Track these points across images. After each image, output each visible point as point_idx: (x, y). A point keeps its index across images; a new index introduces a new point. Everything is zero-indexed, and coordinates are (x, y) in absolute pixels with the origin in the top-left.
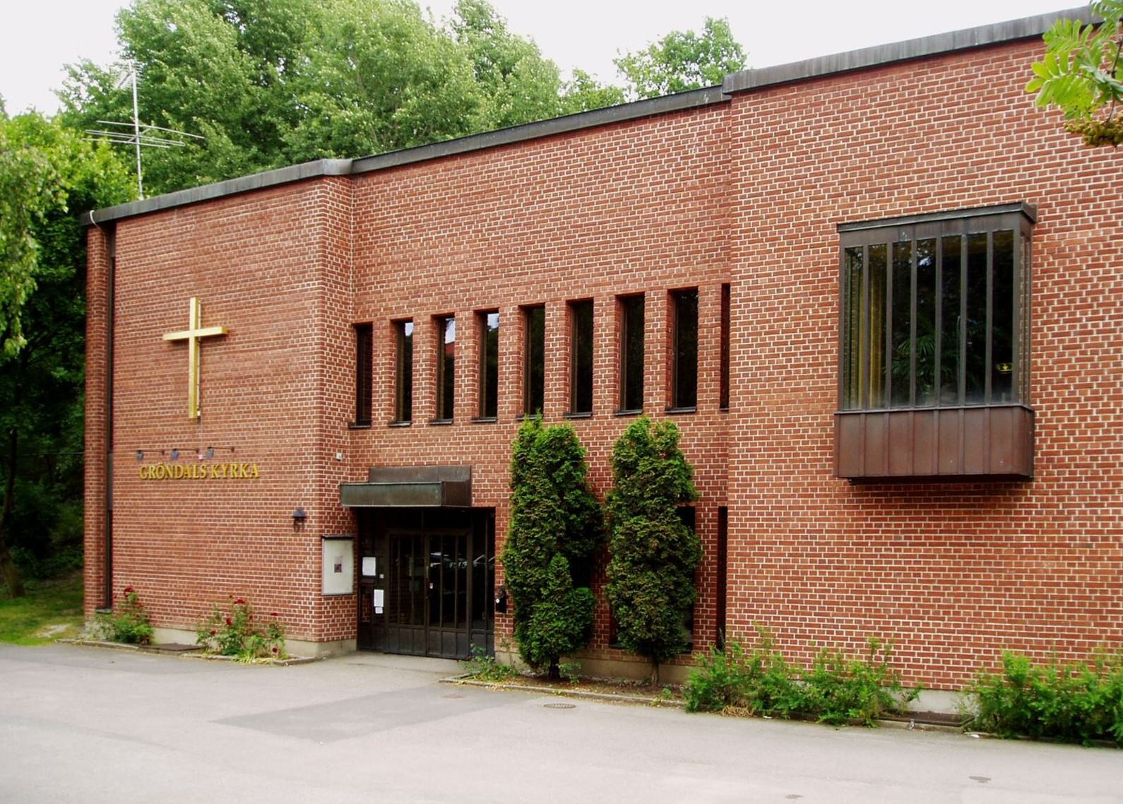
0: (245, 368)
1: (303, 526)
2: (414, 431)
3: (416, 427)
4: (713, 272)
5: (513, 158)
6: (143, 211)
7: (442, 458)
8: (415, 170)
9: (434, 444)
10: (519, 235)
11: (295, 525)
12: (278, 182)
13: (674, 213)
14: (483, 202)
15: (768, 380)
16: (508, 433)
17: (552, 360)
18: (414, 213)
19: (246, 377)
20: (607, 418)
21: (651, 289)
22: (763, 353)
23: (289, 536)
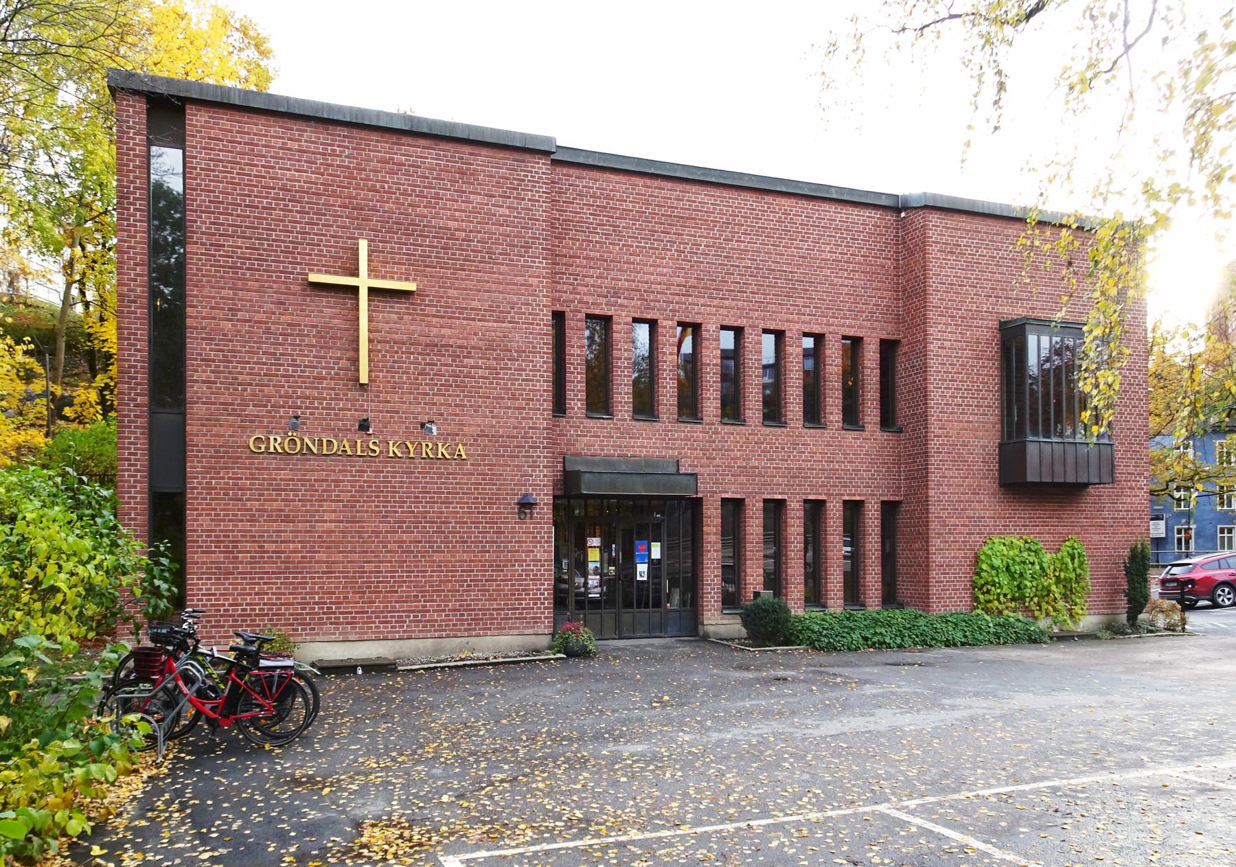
0: (443, 336)
1: (531, 513)
2: (616, 424)
3: (617, 420)
4: (874, 329)
5: (713, 196)
6: (381, 124)
7: (649, 451)
8: (612, 176)
9: (638, 438)
10: (720, 264)
11: (519, 513)
12: (398, 127)
13: (846, 278)
14: (686, 227)
15: (951, 413)
16: (713, 433)
17: (751, 376)
18: (612, 217)
19: (443, 346)
20: (798, 428)
21: (830, 333)
22: (948, 394)
23: (512, 522)
